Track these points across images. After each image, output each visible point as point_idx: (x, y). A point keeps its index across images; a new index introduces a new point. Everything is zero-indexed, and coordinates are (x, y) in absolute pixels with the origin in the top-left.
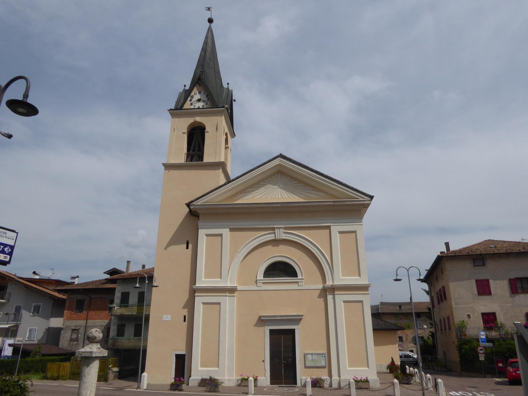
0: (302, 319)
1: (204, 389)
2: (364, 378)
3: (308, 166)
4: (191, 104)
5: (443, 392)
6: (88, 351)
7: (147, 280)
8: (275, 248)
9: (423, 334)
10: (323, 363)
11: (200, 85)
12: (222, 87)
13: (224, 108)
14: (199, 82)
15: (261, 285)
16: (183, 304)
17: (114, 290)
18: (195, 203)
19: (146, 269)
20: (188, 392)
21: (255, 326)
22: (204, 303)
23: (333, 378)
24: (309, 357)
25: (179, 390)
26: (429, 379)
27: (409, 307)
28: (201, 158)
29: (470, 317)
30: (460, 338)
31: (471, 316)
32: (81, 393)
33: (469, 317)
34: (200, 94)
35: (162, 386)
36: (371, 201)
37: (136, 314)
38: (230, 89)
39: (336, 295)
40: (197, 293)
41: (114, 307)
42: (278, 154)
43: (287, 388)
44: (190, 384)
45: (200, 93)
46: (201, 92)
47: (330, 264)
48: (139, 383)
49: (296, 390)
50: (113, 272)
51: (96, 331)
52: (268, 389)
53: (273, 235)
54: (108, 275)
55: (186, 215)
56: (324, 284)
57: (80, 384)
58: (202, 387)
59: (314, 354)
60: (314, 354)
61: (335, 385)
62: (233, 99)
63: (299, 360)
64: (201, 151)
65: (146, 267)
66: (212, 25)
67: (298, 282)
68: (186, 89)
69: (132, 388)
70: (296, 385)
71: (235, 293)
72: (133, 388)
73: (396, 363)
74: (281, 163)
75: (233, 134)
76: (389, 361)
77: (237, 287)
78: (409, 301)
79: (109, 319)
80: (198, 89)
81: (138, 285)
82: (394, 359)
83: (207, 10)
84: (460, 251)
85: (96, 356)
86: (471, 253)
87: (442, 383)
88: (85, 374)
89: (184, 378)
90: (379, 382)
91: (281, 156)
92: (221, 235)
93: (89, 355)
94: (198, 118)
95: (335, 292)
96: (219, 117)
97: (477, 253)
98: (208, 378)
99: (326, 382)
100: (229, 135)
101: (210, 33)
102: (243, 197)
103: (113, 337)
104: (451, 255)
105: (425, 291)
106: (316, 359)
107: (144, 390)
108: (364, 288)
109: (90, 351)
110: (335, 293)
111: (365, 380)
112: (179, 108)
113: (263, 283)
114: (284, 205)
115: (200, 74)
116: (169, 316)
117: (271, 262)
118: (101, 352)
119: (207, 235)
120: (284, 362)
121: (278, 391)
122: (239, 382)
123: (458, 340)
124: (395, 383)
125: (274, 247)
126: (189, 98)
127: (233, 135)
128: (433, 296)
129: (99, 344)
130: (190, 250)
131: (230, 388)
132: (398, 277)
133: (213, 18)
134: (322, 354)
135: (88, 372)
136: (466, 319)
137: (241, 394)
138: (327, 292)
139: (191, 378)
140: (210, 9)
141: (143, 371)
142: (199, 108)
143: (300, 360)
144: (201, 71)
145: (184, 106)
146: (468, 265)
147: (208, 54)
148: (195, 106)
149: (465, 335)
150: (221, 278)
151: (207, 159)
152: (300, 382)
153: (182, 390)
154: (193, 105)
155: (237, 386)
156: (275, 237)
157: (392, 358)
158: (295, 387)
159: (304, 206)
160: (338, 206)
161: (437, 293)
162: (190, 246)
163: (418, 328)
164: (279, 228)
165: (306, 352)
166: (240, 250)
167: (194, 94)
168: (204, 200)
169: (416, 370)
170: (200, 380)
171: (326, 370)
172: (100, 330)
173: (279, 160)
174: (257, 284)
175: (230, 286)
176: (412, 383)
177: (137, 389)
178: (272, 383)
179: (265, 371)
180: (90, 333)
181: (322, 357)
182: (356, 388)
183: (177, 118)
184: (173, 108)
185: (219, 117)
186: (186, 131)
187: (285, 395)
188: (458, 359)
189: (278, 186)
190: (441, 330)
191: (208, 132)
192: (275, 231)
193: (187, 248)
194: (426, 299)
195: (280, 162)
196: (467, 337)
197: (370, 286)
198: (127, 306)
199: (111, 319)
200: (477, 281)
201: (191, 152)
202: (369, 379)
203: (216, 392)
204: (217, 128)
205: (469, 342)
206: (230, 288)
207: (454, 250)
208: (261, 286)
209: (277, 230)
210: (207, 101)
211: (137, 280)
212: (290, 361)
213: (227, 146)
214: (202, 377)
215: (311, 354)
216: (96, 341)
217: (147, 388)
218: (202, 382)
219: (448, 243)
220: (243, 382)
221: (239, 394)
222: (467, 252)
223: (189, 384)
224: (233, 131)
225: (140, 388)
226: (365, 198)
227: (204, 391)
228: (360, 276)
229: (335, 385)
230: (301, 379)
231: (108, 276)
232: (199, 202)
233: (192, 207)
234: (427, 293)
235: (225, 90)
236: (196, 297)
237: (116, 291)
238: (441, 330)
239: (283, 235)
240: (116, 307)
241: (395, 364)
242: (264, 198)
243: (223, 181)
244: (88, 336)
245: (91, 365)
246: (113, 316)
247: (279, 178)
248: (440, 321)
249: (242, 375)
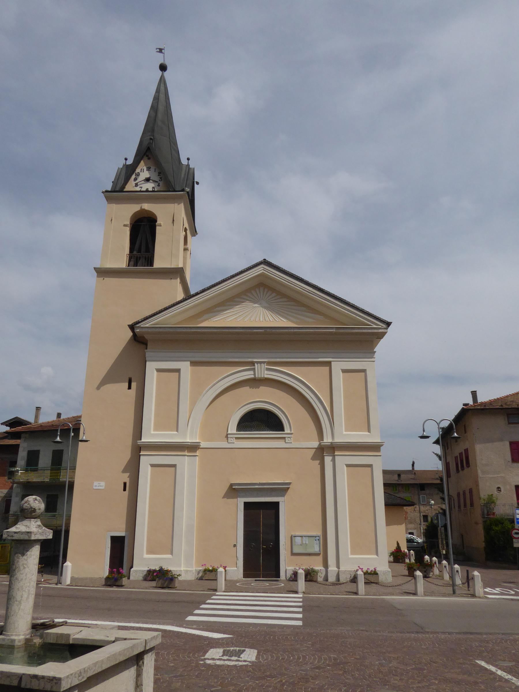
0: (288, 488)
1: (154, 584)
2: (372, 568)
3: (303, 278)
4: (136, 185)
5: (480, 589)
6: (24, 531)
7: (73, 433)
8: (254, 390)
9: (427, 512)
10: (316, 549)
11: (149, 159)
12: (180, 162)
14: (147, 154)
15: (234, 441)
16: (123, 468)
17: (17, 446)
18: (142, 325)
19: (63, 419)
20: (130, 588)
21: (224, 497)
22: (152, 466)
23: (329, 569)
24: (298, 540)
25: (118, 586)
26: (457, 571)
27: (412, 476)
28: (150, 262)
29: (500, 491)
30: (487, 517)
31: (502, 490)
32: (14, 596)
33: (499, 491)
34: (149, 171)
35: (92, 581)
36: (387, 328)
37: (49, 480)
38: (190, 167)
39: (336, 457)
40: (142, 451)
41: (18, 471)
42: (261, 259)
43: (268, 582)
44: (132, 578)
45: (148, 170)
46: (150, 168)
47: (330, 414)
48: (59, 576)
49: (281, 585)
50: (15, 422)
51: (35, 500)
52: (241, 584)
53: (252, 372)
54: (8, 427)
55: (127, 343)
56: (321, 442)
57: (10, 581)
58: (148, 581)
59: (305, 536)
60: (305, 536)
61: (332, 579)
62: (195, 181)
63: (283, 545)
64: (149, 252)
65: (63, 417)
66: (166, 74)
67: (284, 438)
68: (127, 164)
69: (49, 583)
70: (279, 579)
71: (198, 451)
72: (50, 584)
73: (402, 549)
74: (264, 272)
75: (195, 231)
76: (394, 548)
77: (200, 443)
78: (411, 469)
79: (9, 487)
80: (146, 165)
81: (58, 439)
82: (400, 544)
84: (491, 402)
85: (36, 538)
86: (505, 406)
87: (480, 576)
88: (19, 567)
89: (123, 569)
90: (391, 574)
91: (265, 262)
92: (178, 371)
93: (26, 537)
94: (146, 204)
95: (336, 452)
96: (176, 204)
97: (513, 407)
98: (158, 569)
99: (319, 574)
100: (188, 232)
101: (162, 85)
102: (210, 318)
103: (16, 513)
104: (479, 408)
105: (437, 455)
106: (307, 543)
107: (68, 585)
108: (375, 448)
109: (28, 531)
110: (335, 454)
111: (373, 572)
112: (117, 189)
113: (236, 438)
114: (268, 330)
115: (149, 143)
116: (103, 484)
117: (245, 411)
118: (43, 532)
119: (158, 370)
120: (263, 547)
121: (257, 586)
122: (200, 575)
123: (483, 520)
124: (417, 576)
125: (253, 388)
126: (133, 177)
127: (194, 233)
128: (449, 463)
129: (39, 519)
130: (133, 392)
131: (188, 582)
132: (425, 433)
133: (166, 63)
134: (316, 537)
135: (23, 564)
136: (495, 492)
137: (206, 591)
138: (325, 452)
139: (132, 569)
140: (163, 51)
141: (65, 560)
142: (147, 191)
143: (285, 544)
144: (151, 139)
145: (126, 187)
146: (501, 421)
147: (160, 116)
148: (141, 187)
149: (494, 514)
150: (177, 431)
151: (158, 263)
152: (285, 575)
153: (122, 586)
154: (139, 187)
155: (197, 579)
156: (255, 374)
157: (397, 542)
158: (277, 581)
159: (295, 333)
160: (343, 334)
161: (455, 457)
162: (134, 385)
163: (421, 504)
164: (261, 363)
165: (293, 534)
166: (204, 392)
167: (140, 170)
168: (156, 321)
169: (434, 559)
170: (146, 572)
171: (320, 558)
172: (40, 498)
173: (263, 268)
174: (228, 439)
175: (190, 441)
176: (430, 576)
177: (56, 584)
178: (245, 575)
179: (237, 559)
180: (26, 502)
181: (316, 540)
182: (365, 583)
184: (109, 189)
185: (177, 204)
186: (128, 223)
187: (269, 592)
188: (482, 545)
189: (260, 304)
190: (459, 507)
192: (254, 367)
193: (130, 388)
194: (437, 465)
195: (263, 271)
196: (495, 517)
197: (383, 445)
198: (36, 470)
199: (12, 488)
200: (511, 443)
201: (135, 253)
202: (378, 571)
203: (170, 588)
204: (173, 220)
205: (500, 522)
206: (190, 444)
207: (483, 401)
208: (234, 443)
209: (257, 365)
210: (158, 181)
211: (58, 433)
212: (271, 546)
213: (186, 247)
214: (150, 568)
215: (301, 536)
216: (35, 515)
217: (71, 583)
218: (149, 574)
219: (476, 391)
220: (206, 574)
221: (204, 591)
222: (500, 404)
223: (130, 578)
224: (193, 225)
225: (61, 583)
226: (380, 325)
227: (153, 587)
228: (369, 431)
229: (332, 579)
230: (286, 569)
231: (8, 429)
232: (148, 324)
233: (138, 330)
234: (439, 458)
235: (184, 169)
236: (141, 457)
237: (21, 449)
238: (459, 507)
239: (266, 372)
240: (19, 471)
241: (401, 551)
242: (240, 320)
243: (181, 296)
244: (23, 507)
245: (28, 553)
246: (16, 484)
247: (262, 293)
248: (459, 494)
249: (205, 565)
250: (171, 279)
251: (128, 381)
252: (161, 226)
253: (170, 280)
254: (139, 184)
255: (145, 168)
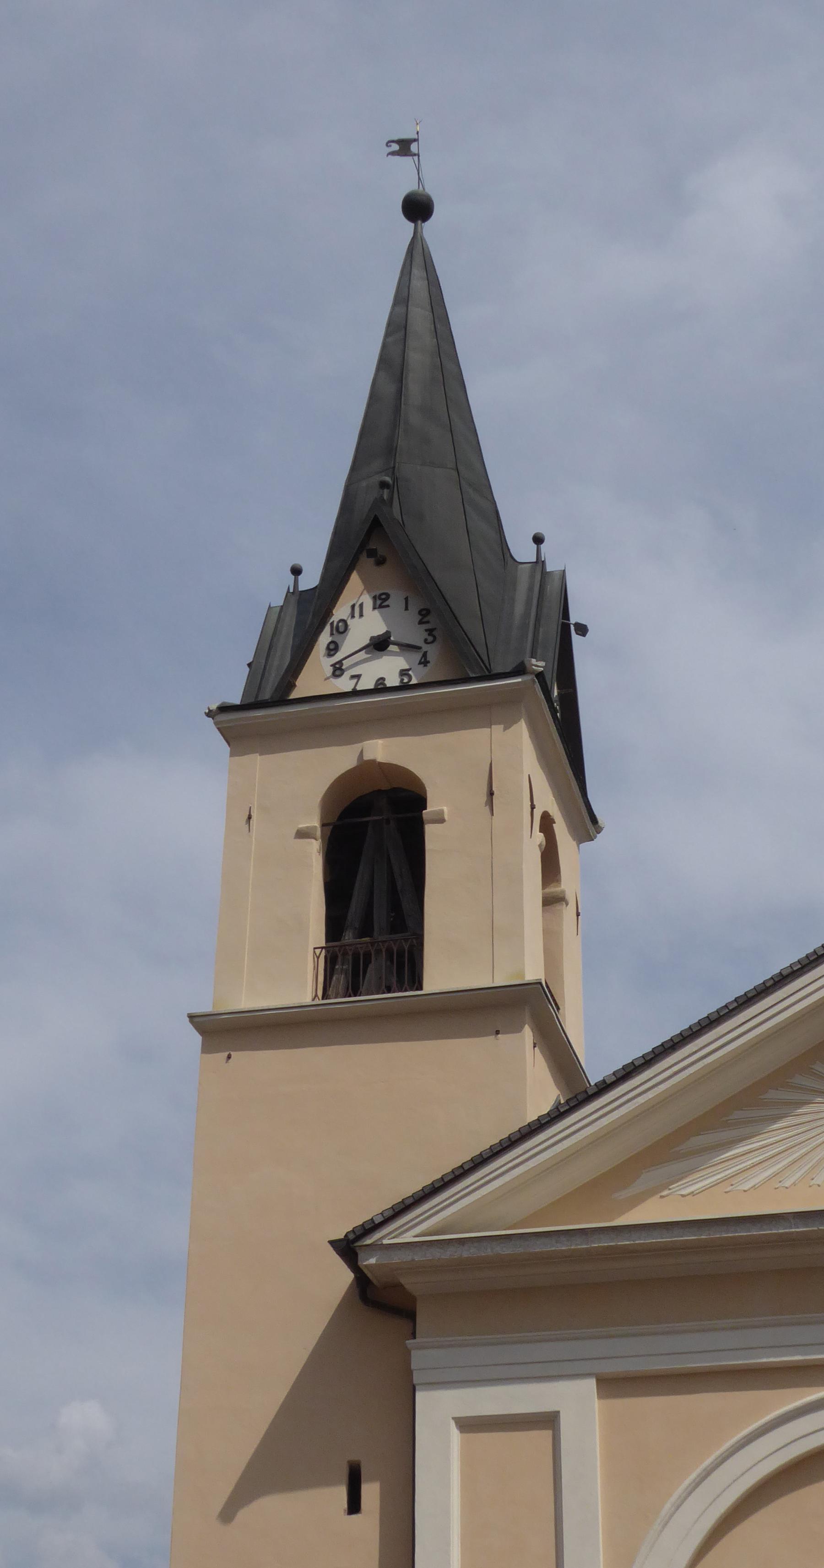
4: (338, 670)
13: (527, 678)
45: (381, 607)
46: (388, 596)
80: (368, 586)
83: (393, 153)
102: (666, 1186)
126: (325, 638)
140: (414, 147)
142: (381, 688)
148: (358, 677)
183: (261, 754)
186: (314, 821)
191: (440, 819)
193: (354, 1506)
204: (491, 794)
250: (497, 1032)
251: (344, 1473)
252: (441, 821)
253: (492, 1038)
254: (346, 664)
255: (367, 601)
